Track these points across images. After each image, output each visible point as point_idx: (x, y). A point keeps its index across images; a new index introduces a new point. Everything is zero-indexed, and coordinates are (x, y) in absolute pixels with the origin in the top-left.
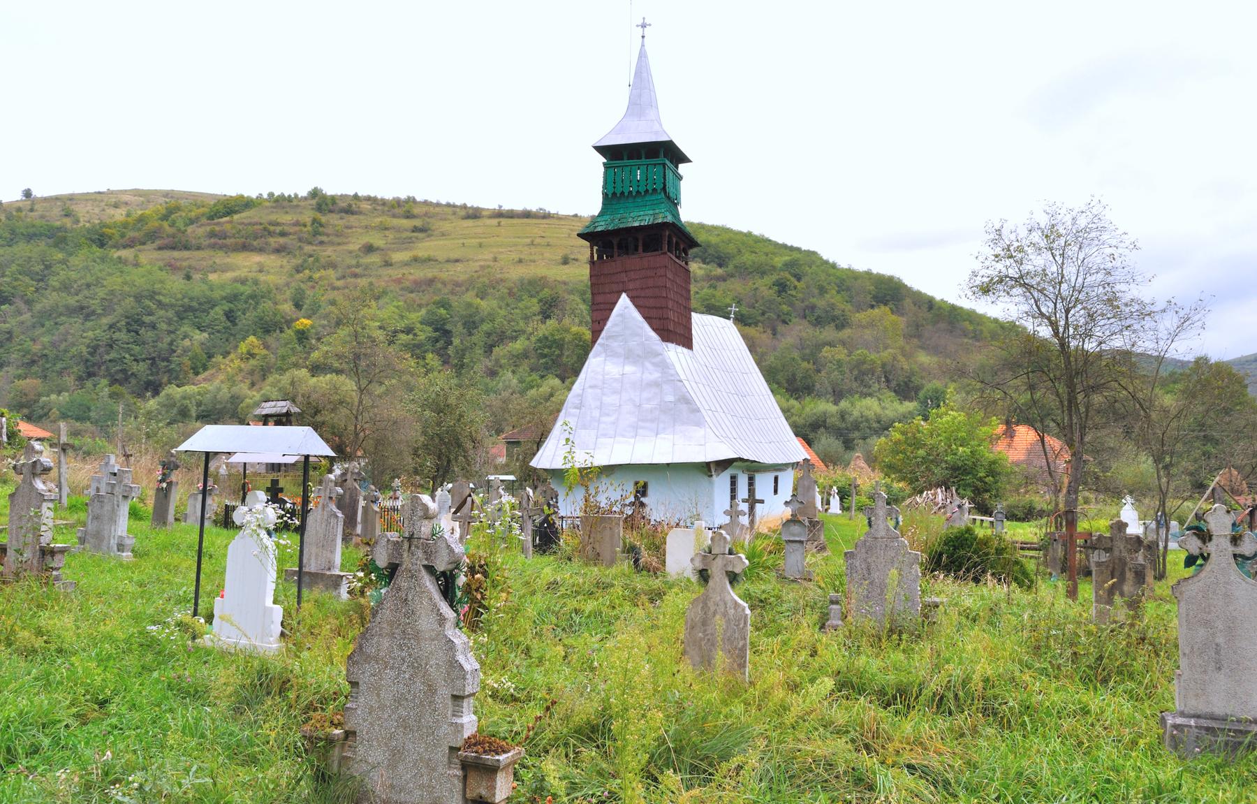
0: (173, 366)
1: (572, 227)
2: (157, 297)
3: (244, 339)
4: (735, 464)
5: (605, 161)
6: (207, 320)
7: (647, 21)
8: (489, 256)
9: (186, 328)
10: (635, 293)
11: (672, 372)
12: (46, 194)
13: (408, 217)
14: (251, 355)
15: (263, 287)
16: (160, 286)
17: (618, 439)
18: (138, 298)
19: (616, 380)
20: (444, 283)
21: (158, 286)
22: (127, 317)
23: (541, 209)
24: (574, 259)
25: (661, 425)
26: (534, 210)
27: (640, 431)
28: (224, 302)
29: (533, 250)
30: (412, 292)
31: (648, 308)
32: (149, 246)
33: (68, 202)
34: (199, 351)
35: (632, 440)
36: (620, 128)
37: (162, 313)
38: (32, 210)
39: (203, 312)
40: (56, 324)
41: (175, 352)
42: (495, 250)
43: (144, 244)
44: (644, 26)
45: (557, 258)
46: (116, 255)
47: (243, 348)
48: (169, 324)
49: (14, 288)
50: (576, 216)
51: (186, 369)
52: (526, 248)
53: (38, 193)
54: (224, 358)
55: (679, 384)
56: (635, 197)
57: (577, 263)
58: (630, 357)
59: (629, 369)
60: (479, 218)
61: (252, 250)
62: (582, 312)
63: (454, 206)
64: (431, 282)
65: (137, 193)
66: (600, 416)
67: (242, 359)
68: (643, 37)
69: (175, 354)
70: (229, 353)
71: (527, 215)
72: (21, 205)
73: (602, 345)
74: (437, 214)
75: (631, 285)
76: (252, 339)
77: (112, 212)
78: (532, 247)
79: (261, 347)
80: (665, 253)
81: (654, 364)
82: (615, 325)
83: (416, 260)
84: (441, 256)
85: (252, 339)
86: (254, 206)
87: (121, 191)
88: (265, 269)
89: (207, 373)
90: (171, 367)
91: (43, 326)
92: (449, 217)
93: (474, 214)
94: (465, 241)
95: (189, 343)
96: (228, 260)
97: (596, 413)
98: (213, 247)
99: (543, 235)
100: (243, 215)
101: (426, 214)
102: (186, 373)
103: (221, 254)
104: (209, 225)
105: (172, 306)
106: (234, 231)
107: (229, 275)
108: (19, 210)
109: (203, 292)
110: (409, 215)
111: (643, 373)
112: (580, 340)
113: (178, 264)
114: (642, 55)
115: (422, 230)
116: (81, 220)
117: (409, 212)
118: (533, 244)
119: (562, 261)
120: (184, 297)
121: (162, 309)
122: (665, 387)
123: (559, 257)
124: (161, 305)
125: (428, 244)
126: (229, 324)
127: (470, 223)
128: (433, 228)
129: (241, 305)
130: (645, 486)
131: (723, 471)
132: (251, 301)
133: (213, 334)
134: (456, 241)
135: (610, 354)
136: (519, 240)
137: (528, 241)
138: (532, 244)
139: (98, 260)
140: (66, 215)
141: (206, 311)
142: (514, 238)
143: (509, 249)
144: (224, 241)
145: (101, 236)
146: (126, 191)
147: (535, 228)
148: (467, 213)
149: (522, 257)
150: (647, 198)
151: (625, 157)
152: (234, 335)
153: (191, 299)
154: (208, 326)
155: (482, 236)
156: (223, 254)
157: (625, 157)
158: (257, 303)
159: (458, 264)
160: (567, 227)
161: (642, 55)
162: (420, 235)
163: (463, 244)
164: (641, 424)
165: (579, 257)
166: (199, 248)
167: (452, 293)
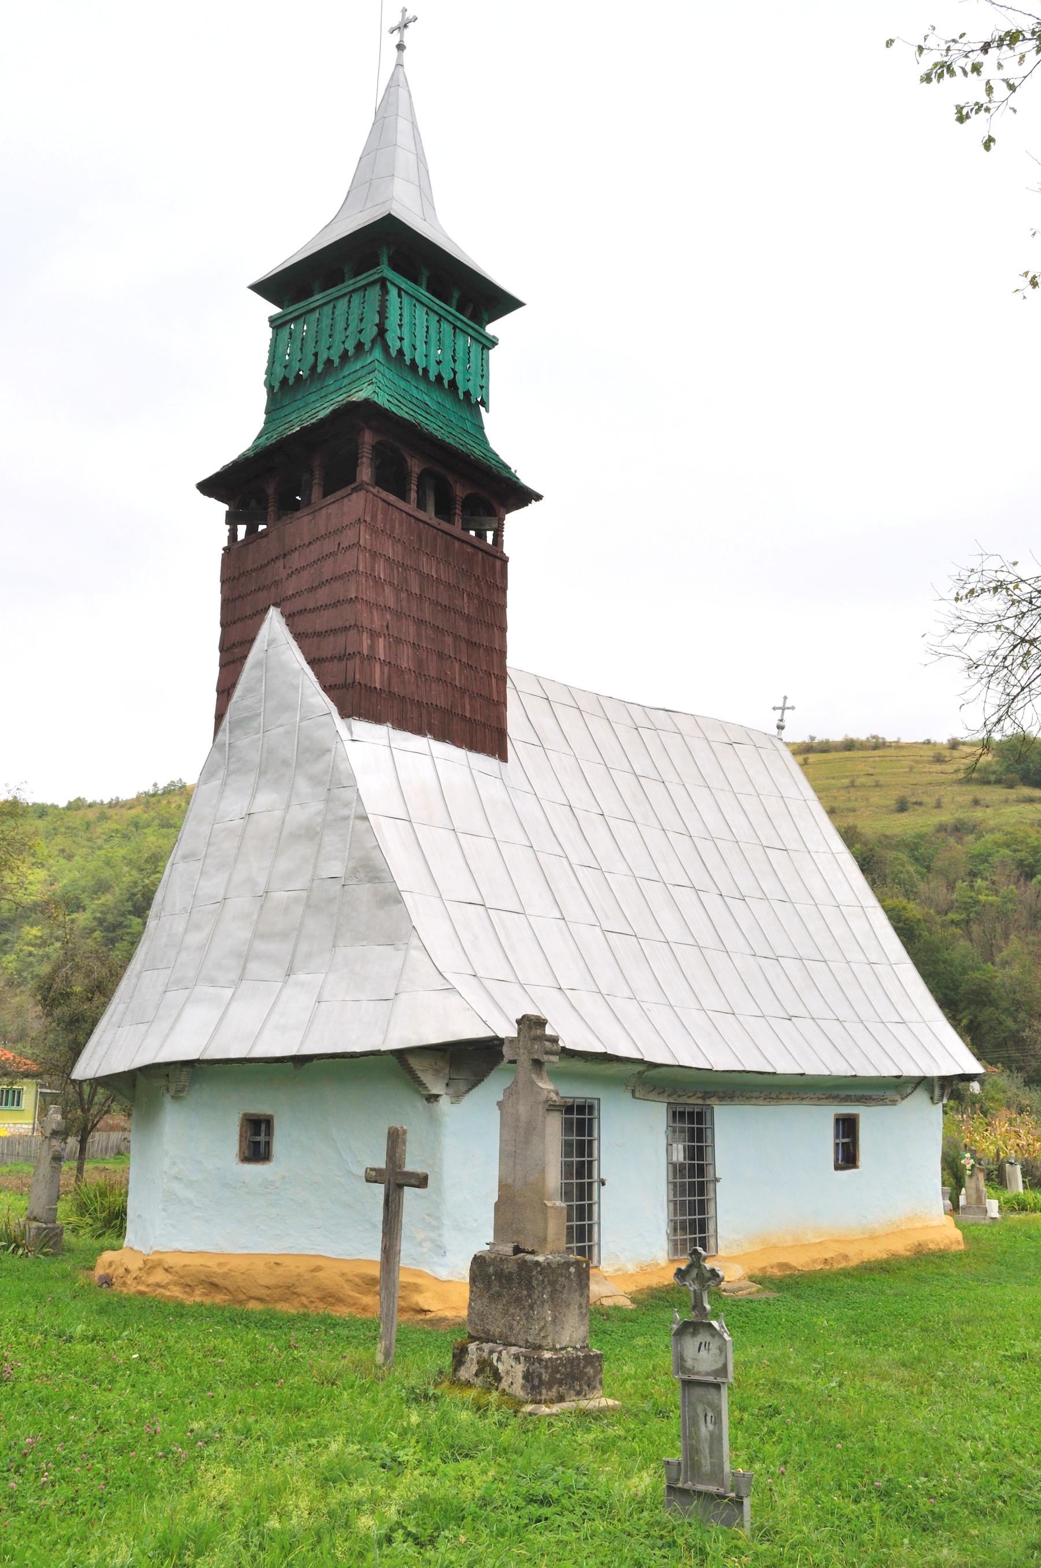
1: (918, 758)
5: (275, 310)
11: (347, 794)
17: (203, 990)
23: (874, 737)
24: (916, 803)
25: (304, 947)
45: (889, 803)
50: (928, 742)
52: (842, 792)
55: (361, 825)
57: (920, 809)
62: (911, 877)
71: (849, 745)
78: (852, 790)
82: (249, 690)
97: (179, 926)
99: (871, 771)
114: (396, 83)
119: (894, 807)
123: (892, 803)
136: (833, 781)
137: (846, 781)
138: (852, 785)
142: (827, 778)
149: (835, 805)
160: (911, 758)
161: (396, 83)
164: (260, 946)
165: (925, 799)
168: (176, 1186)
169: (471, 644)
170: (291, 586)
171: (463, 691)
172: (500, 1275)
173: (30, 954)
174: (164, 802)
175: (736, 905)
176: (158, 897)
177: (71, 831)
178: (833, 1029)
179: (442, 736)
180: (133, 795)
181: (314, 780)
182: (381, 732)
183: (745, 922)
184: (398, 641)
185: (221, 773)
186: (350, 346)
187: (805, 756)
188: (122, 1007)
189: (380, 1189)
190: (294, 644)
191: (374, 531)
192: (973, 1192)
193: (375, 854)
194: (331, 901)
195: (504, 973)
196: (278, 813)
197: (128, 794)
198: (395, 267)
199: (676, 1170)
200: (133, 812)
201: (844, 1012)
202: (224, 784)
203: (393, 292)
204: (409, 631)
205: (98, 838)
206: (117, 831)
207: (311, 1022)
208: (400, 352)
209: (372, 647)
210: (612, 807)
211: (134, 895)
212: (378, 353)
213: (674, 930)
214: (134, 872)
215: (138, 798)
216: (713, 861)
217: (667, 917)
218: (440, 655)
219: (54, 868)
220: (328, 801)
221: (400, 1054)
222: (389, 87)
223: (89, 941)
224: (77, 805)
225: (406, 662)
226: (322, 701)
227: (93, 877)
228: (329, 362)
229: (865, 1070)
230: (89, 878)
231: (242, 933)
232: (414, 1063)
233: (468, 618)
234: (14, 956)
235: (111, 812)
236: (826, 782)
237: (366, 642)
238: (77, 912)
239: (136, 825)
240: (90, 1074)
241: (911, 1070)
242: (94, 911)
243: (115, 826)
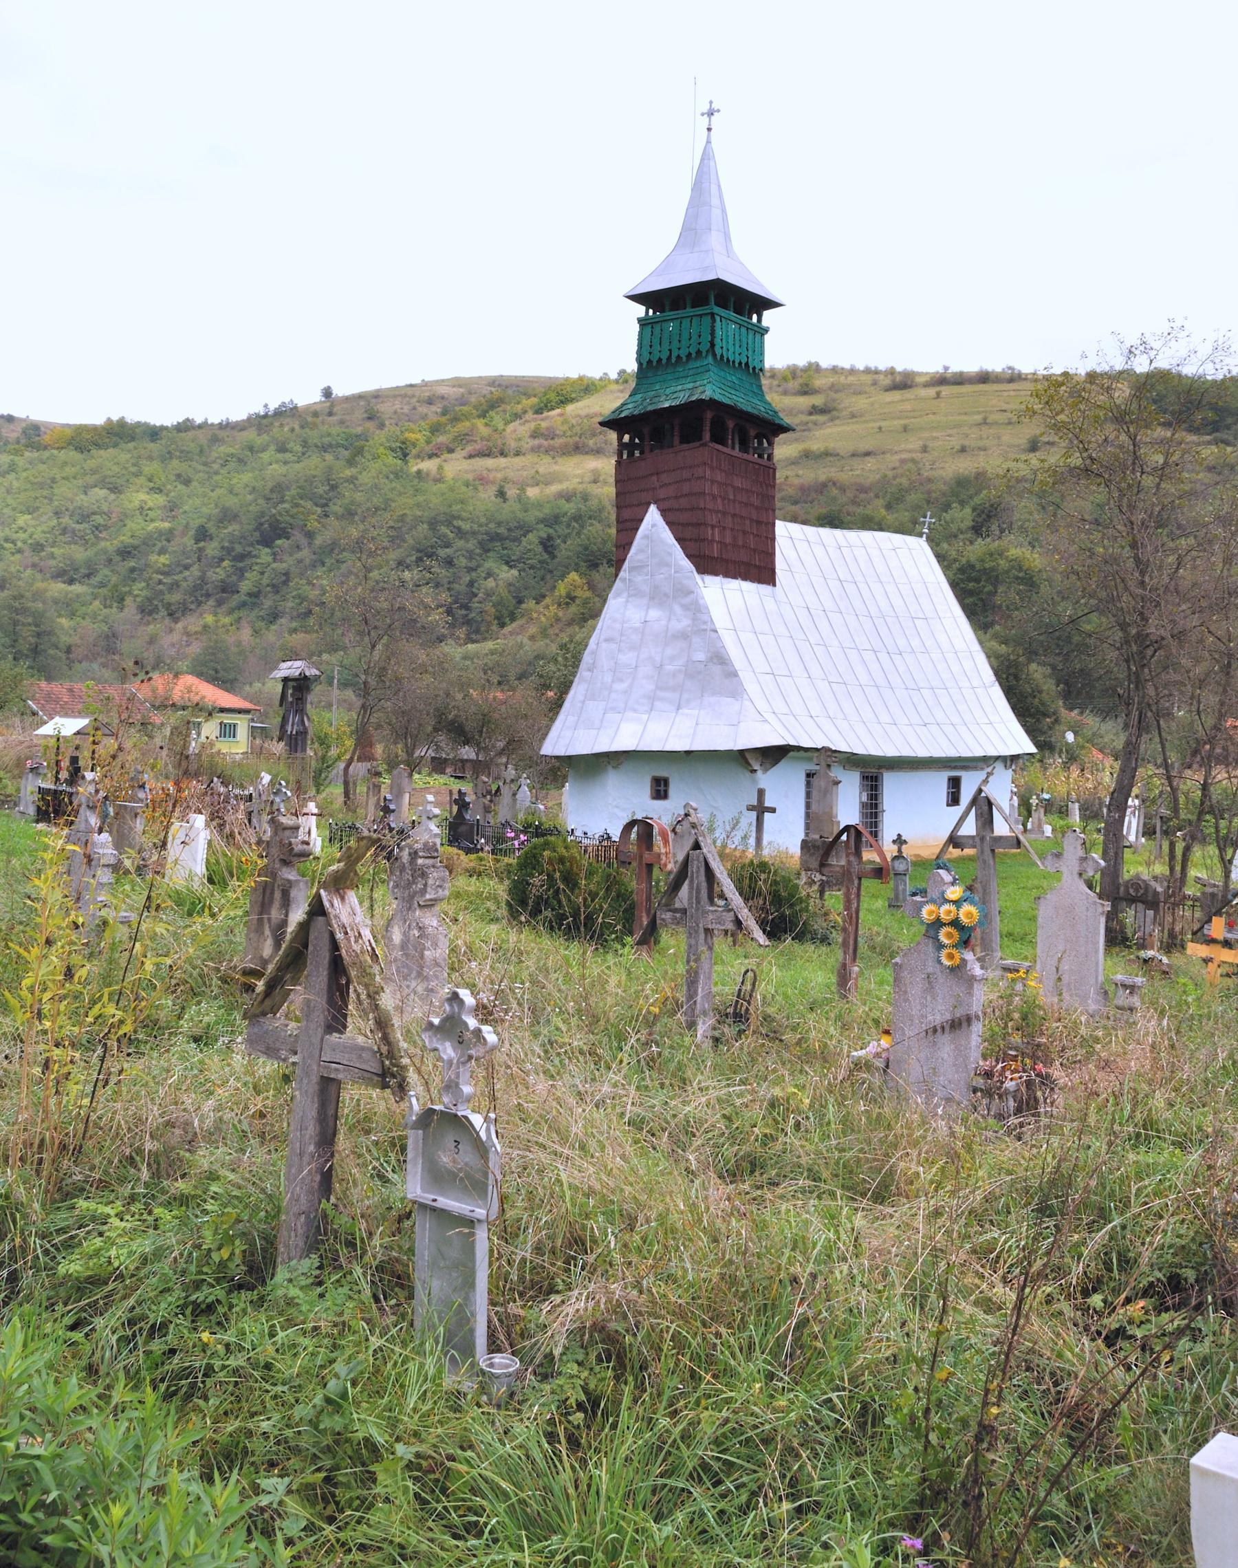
0: (472, 615)
2: (455, 523)
3: (563, 577)
4: (791, 754)
6: (516, 551)
7: (715, 106)
9: (490, 564)
10: (667, 505)
11: (705, 617)
13: (805, 393)
15: (593, 503)
16: (459, 507)
17: (629, 714)
18: (433, 524)
19: (636, 630)
20: (843, 489)
23: (1010, 368)
24: (1048, 443)
25: (686, 696)
26: (999, 369)
28: (541, 526)
29: (985, 431)
30: (796, 503)
32: (460, 454)
33: (374, 400)
35: (645, 717)
36: (668, 263)
37: (460, 543)
38: (330, 414)
41: (476, 596)
42: (926, 434)
44: (711, 113)
45: (1021, 441)
46: (415, 469)
47: (562, 589)
48: (470, 559)
49: (292, 516)
51: (489, 619)
53: (339, 391)
55: (714, 635)
58: (657, 597)
59: (654, 614)
60: (911, 387)
61: (587, 453)
63: (877, 372)
64: (822, 488)
65: (457, 382)
66: (613, 682)
67: (559, 605)
68: (709, 129)
69: (476, 599)
70: (544, 596)
71: (984, 378)
72: (318, 408)
73: (624, 580)
74: (850, 385)
75: (662, 493)
76: (574, 576)
79: (586, 588)
80: (705, 445)
82: (641, 551)
84: (844, 447)
85: (574, 576)
86: (597, 391)
87: (437, 381)
89: (514, 625)
91: (323, 564)
92: (868, 389)
93: (902, 382)
94: (883, 424)
95: (493, 584)
96: (556, 468)
97: (608, 678)
98: (535, 450)
99: (1005, 407)
100: (580, 404)
101: (832, 387)
102: (489, 624)
103: (547, 459)
104: (535, 420)
105: (474, 533)
107: (555, 488)
108: (316, 414)
110: (806, 391)
112: (1020, 569)
113: (491, 476)
114: (707, 156)
115: (822, 411)
116: (387, 423)
117: (807, 385)
118: (985, 423)
120: (490, 521)
121: (461, 538)
122: (696, 640)
124: (460, 533)
126: (546, 556)
127: (896, 395)
128: (840, 407)
129: (562, 530)
130: (666, 782)
132: (574, 524)
133: (524, 570)
134: (871, 425)
135: (635, 593)
136: (965, 418)
137: (978, 418)
138: (984, 422)
139: (392, 476)
140: (369, 418)
141: (517, 540)
142: (960, 414)
143: (950, 432)
144: (552, 442)
145: (404, 443)
146: (443, 381)
147: (992, 398)
148: (893, 381)
149: (966, 443)
150: (692, 364)
151: (689, 303)
152: (551, 572)
153: (499, 524)
154: (518, 561)
156: (551, 461)
157: (689, 303)
158: (582, 527)
161: (707, 156)
162: (820, 418)
163: (880, 428)
166: (517, 454)
167: (854, 502)
168: (616, 810)
169: (759, 522)
170: (662, 493)
171: (755, 550)
172: (814, 846)
173: (160, 582)
174: (277, 424)
175: (897, 658)
176: (587, 658)
177: (186, 456)
178: (949, 729)
180: (245, 417)
181: (685, 608)
182: (718, 580)
183: (902, 669)
184: (724, 528)
185: (625, 595)
186: (693, 351)
187: (938, 389)
190: (667, 528)
191: (712, 468)
192: (1036, 821)
193: (722, 650)
194: (699, 673)
195: (786, 710)
196: (664, 622)
198: (717, 304)
199: (863, 805)
200: (245, 434)
201: (955, 719)
202: (627, 601)
203: (718, 318)
204: (728, 522)
205: (214, 462)
206: (232, 455)
207: (694, 734)
208: (722, 356)
209: (713, 534)
210: (829, 604)
211: (262, 524)
212: (710, 359)
213: (864, 678)
214: (261, 501)
215: (249, 419)
216: (883, 630)
218: (744, 532)
219: (173, 494)
220: (694, 620)
221: (742, 753)
222: (702, 160)
223: (218, 570)
224: (185, 427)
225: (728, 540)
226: (686, 564)
227: (216, 505)
228: (679, 357)
229: (966, 753)
231: (649, 686)
232: (748, 756)
233: (757, 508)
234: (143, 584)
237: (710, 532)
238: (204, 540)
239: (251, 449)
243: (232, 450)
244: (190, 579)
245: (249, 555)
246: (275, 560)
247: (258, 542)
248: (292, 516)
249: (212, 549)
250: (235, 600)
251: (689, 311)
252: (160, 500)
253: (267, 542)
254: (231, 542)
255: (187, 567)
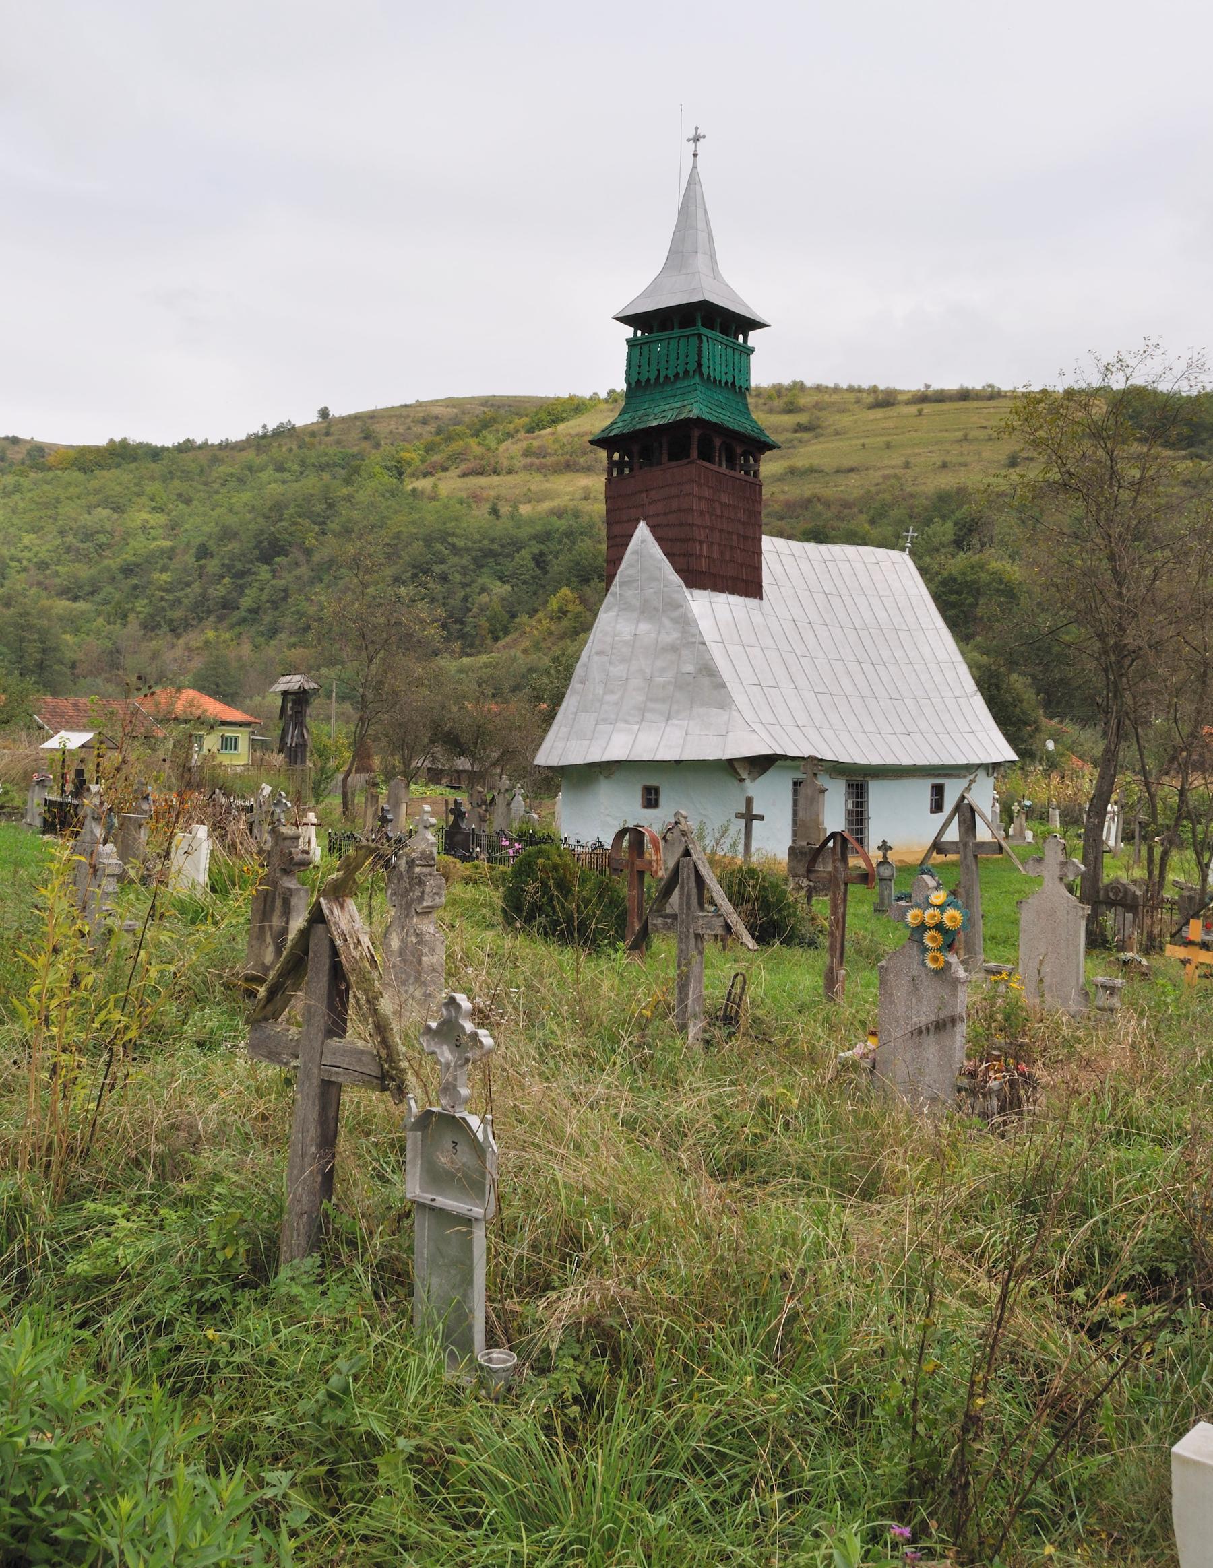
2: (450, 539)
3: (555, 592)
4: (779, 763)
6: (509, 567)
8: (898, 461)
9: (484, 579)
11: (694, 630)
12: (345, 413)
13: (790, 411)
14: (564, 612)
17: (621, 725)
18: (428, 541)
20: (827, 505)
21: (450, 525)
22: (414, 567)
23: (989, 386)
24: (1027, 459)
25: (675, 707)
26: (979, 387)
27: (648, 715)
30: (781, 518)
31: (671, 540)
32: (453, 473)
34: (498, 608)
35: (636, 727)
37: (455, 560)
38: (327, 434)
39: (507, 557)
40: (335, 578)
41: (470, 610)
42: (909, 451)
43: (445, 469)
44: (696, 139)
45: (1000, 457)
46: (410, 487)
47: (554, 603)
48: (465, 574)
49: (290, 534)
51: (483, 633)
53: (336, 412)
54: (530, 617)
55: (702, 647)
56: (663, 385)
58: (646, 610)
59: (644, 627)
60: (893, 405)
61: (577, 471)
63: (860, 390)
64: (807, 503)
65: (450, 402)
66: (605, 693)
67: (552, 619)
68: (695, 155)
70: (536, 611)
71: (964, 395)
72: (315, 428)
75: (651, 510)
76: (565, 591)
77: (420, 430)
78: (965, 444)
80: (692, 462)
81: (673, 620)
82: (630, 566)
83: (792, 473)
84: (828, 463)
85: (565, 591)
86: (587, 410)
88: (592, 496)
89: (508, 639)
90: (465, 630)
91: (321, 581)
92: (851, 407)
93: (885, 400)
94: (866, 441)
95: (487, 599)
96: (548, 485)
98: (527, 468)
99: (985, 424)
102: (483, 638)
103: (539, 477)
105: (468, 550)
106: (557, 446)
107: (546, 505)
108: (313, 435)
109: (506, 529)
110: (790, 409)
111: (659, 632)
112: (1001, 582)
114: (693, 181)
117: (792, 403)
118: (966, 439)
122: (684, 652)
123: (1003, 458)
124: (455, 549)
125: (814, 448)
126: (538, 571)
127: (879, 413)
129: (554, 546)
131: (761, 774)
132: (565, 540)
134: (854, 442)
136: (946, 434)
137: (959, 435)
138: (965, 438)
139: (387, 495)
140: (365, 438)
141: (510, 556)
142: (941, 431)
143: (931, 448)
144: (543, 460)
145: (399, 462)
148: (876, 399)
149: (948, 459)
150: (679, 384)
151: (676, 325)
152: (543, 587)
153: (493, 541)
154: (511, 576)
155: (894, 431)
157: (676, 325)
158: (574, 543)
159: (852, 475)
161: (693, 181)
163: (863, 445)
164: (650, 705)
166: (510, 472)
167: (839, 517)
168: (608, 819)
171: (742, 565)
172: (801, 853)
173: (162, 599)
174: (275, 444)
175: (880, 669)
178: (932, 738)
179: (733, 591)
180: (244, 437)
181: (675, 621)
184: (712, 543)
186: (680, 370)
187: (919, 406)
188: (564, 730)
189: (743, 822)
193: (711, 662)
195: (773, 721)
196: (653, 636)
197: (237, 435)
198: (704, 325)
199: (849, 813)
200: (244, 454)
201: (939, 729)
203: (704, 339)
205: (214, 482)
206: (232, 475)
207: (684, 744)
208: (709, 376)
211: (261, 542)
212: (697, 378)
213: (848, 688)
214: (260, 520)
215: (248, 439)
216: (868, 643)
217: (846, 682)
219: (174, 513)
221: (730, 762)
222: (689, 184)
224: (186, 447)
226: (675, 578)
228: (667, 377)
230: (213, 524)
231: (640, 698)
232: (736, 765)
233: (744, 524)
234: (146, 601)
235: (222, 454)
236: (940, 435)
240: (554, 761)
241: (975, 760)
242: (223, 557)
243: (231, 470)
244: (192, 596)
245: (249, 572)
246: (274, 577)
247: (258, 560)
248: (290, 534)
249: (213, 566)
250: (236, 616)
251: (677, 332)
252: (162, 519)
253: (266, 559)
254: (231, 559)
255: (188, 585)
